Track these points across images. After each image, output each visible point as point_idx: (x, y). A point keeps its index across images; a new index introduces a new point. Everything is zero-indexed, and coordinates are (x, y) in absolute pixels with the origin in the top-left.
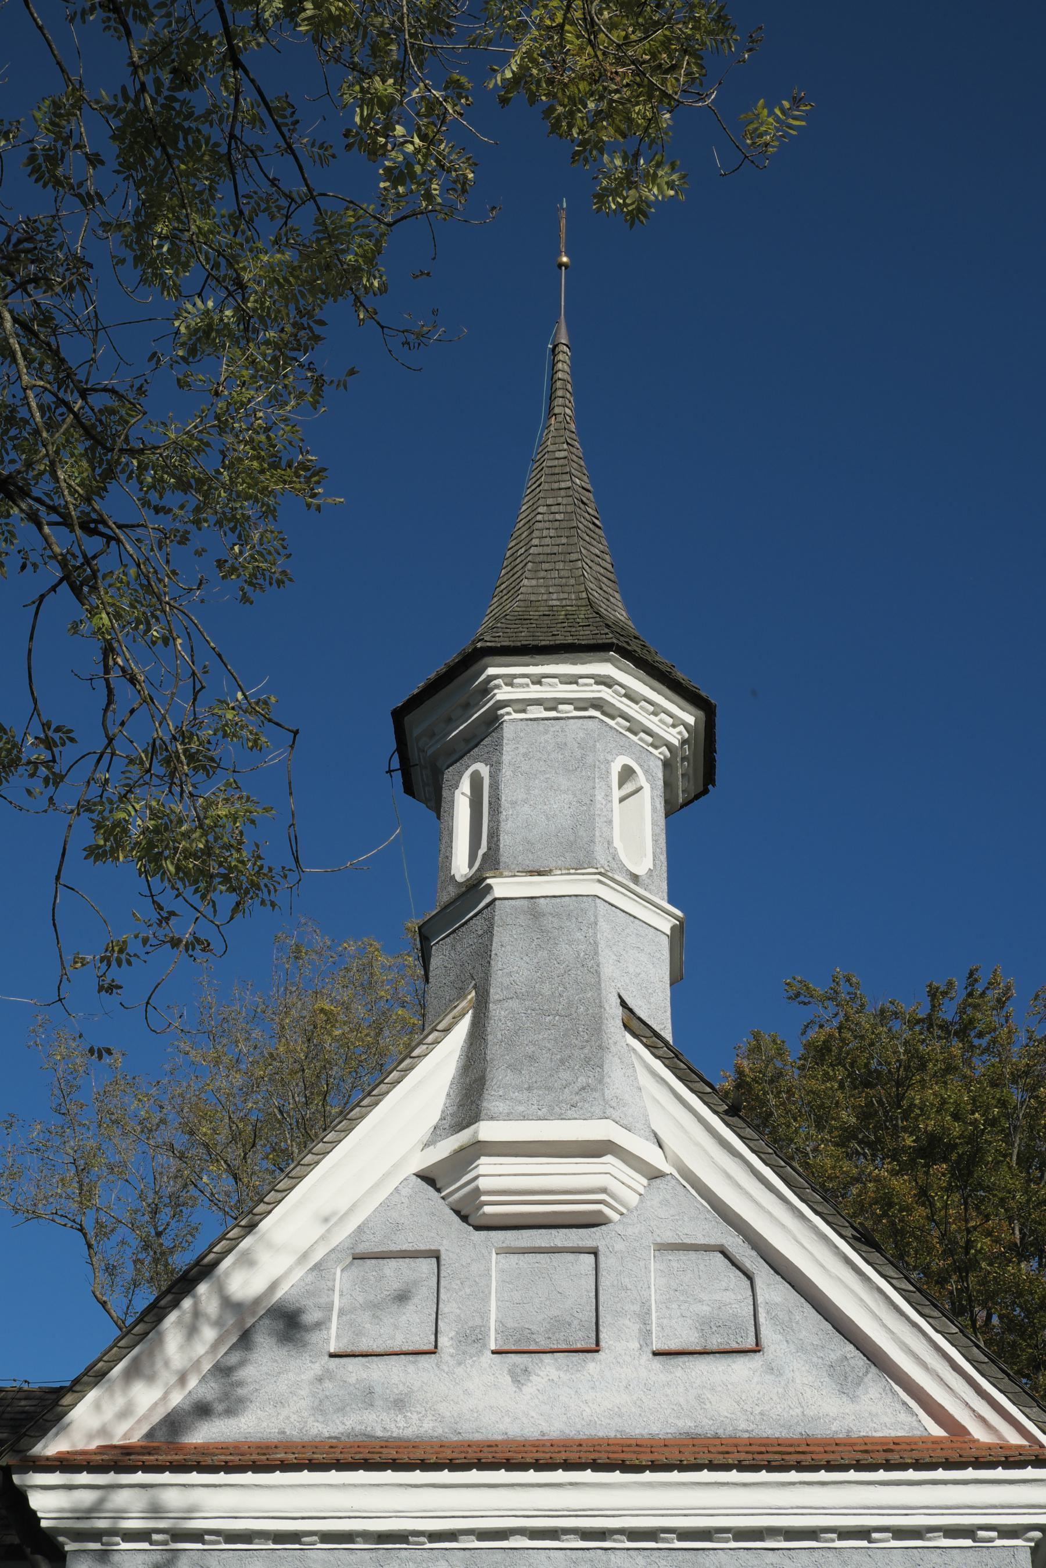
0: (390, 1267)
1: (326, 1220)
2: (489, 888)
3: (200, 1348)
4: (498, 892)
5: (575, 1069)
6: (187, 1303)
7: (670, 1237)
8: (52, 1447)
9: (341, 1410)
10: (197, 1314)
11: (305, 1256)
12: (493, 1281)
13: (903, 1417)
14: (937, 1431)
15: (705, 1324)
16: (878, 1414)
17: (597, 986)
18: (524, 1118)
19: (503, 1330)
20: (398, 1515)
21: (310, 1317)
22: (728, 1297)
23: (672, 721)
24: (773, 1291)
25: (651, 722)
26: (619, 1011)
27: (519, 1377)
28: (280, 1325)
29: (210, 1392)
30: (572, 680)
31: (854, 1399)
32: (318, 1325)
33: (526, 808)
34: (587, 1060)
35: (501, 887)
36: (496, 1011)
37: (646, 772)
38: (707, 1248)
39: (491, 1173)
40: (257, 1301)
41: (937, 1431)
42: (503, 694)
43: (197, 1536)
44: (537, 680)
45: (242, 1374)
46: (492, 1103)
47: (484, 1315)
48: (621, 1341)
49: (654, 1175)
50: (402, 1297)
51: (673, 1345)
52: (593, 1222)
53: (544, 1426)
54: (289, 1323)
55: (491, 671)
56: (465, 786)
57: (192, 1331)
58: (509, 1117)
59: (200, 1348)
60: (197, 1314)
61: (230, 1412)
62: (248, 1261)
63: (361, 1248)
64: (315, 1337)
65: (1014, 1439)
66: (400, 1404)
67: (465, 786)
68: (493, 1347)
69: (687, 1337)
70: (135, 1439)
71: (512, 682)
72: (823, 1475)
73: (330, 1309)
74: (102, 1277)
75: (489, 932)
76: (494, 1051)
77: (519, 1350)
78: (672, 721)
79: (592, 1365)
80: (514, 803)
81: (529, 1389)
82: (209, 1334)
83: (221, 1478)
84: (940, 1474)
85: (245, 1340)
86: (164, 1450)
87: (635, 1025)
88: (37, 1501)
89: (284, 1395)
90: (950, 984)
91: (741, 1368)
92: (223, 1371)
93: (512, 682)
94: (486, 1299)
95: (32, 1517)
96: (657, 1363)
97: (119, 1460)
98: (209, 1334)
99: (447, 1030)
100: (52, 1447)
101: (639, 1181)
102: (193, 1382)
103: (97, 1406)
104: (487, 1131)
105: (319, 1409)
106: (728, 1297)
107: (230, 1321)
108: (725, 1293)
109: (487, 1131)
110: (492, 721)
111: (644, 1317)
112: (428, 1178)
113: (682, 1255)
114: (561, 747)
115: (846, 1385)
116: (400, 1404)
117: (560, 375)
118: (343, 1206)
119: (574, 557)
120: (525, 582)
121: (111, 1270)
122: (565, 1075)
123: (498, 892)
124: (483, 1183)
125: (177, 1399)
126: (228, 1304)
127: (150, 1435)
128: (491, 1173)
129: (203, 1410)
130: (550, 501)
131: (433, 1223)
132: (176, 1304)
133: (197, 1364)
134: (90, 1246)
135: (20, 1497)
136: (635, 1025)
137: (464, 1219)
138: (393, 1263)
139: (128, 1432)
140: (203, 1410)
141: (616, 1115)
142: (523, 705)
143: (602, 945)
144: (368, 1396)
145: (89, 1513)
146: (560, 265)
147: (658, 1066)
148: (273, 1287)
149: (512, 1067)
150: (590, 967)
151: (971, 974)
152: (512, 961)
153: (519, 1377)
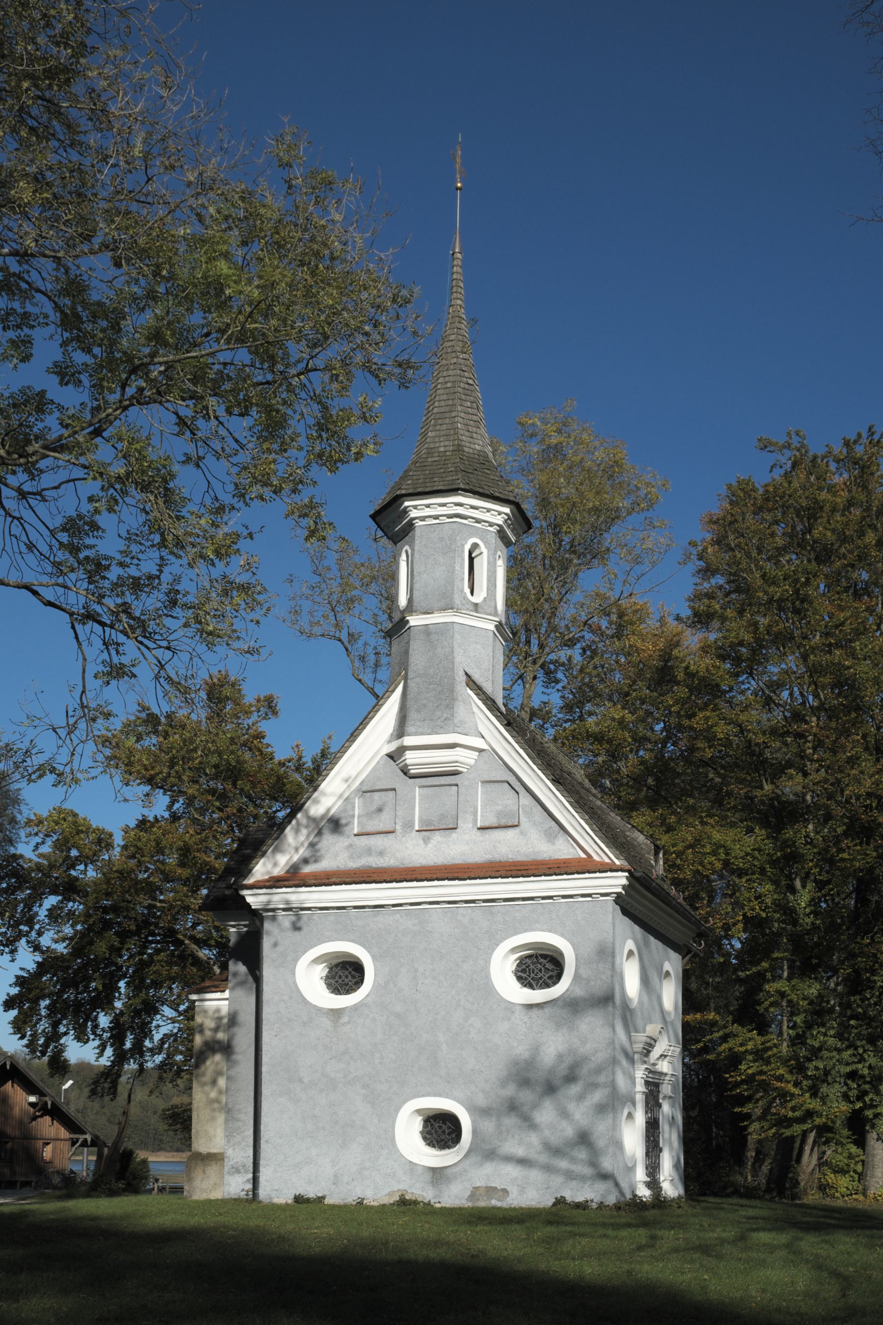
0: (376, 795)
1: (347, 781)
2: (408, 621)
3: (302, 838)
4: (412, 623)
5: (442, 713)
6: (294, 822)
7: (487, 778)
8: (250, 881)
9: (359, 857)
10: (298, 824)
11: (341, 796)
12: (418, 801)
13: (571, 850)
14: (583, 856)
15: (499, 814)
16: (562, 850)
17: (453, 669)
18: (422, 734)
19: (421, 820)
20: (378, 899)
21: (343, 822)
22: (509, 802)
23: (497, 514)
24: (525, 799)
25: (487, 517)
26: (464, 678)
27: (426, 841)
28: (331, 825)
29: (307, 854)
30: (444, 505)
31: (553, 844)
32: (346, 825)
33: (425, 576)
34: (447, 706)
35: (414, 621)
36: (411, 683)
37: (485, 543)
38: (502, 782)
39: (411, 757)
40: (323, 817)
41: (583, 856)
42: (413, 514)
43: (309, 909)
44: (428, 506)
45: (319, 846)
46: (410, 728)
47: (413, 815)
48: (466, 825)
49: (481, 751)
50: (380, 810)
51: (487, 824)
52: (455, 773)
53: (436, 860)
54: (335, 824)
55: (407, 504)
56: (404, 557)
57: (297, 831)
58: (416, 734)
59: (302, 838)
60: (298, 824)
61: (316, 861)
62: (316, 802)
63: (364, 789)
64: (347, 829)
65: (607, 860)
66: (381, 853)
67: (404, 557)
68: (417, 828)
69: (492, 821)
70: (282, 873)
71: (418, 509)
72: (532, 878)
73: (353, 816)
74: (357, 663)
75: (408, 642)
76: (410, 703)
77: (428, 830)
78: (497, 514)
79: (454, 835)
80: (419, 573)
81: (430, 846)
82: (304, 832)
83: (313, 889)
84: (576, 876)
85: (320, 833)
86: (294, 878)
87: (471, 683)
88: (249, 899)
89: (336, 854)
90: (859, 435)
91: (511, 833)
92: (312, 845)
93: (418, 509)
94: (414, 808)
95: (249, 905)
96: (479, 833)
97: (275, 883)
98: (304, 832)
99: (393, 691)
100: (250, 881)
101: (475, 755)
102: (301, 851)
103: (264, 864)
104: (408, 741)
105: (351, 857)
106: (509, 802)
107: (313, 826)
108: (507, 800)
109: (408, 741)
110: (410, 525)
111: (475, 814)
112: (391, 756)
113: (492, 785)
114: (442, 539)
115: (550, 837)
116: (381, 853)
117: (455, 276)
118: (354, 774)
119: (454, 414)
120: (430, 434)
121: (362, 659)
122: (438, 713)
123: (412, 623)
124: (408, 762)
125: (296, 858)
126: (314, 820)
127: (287, 872)
128: (411, 757)
129: (306, 861)
130: (445, 374)
131: (392, 776)
132: (290, 822)
133: (302, 844)
134: (347, 649)
135: (243, 898)
136: (471, 683)
137: (405, 774)
138: (378, 794)
139: (277, 872)
140: (306, 861)
141: (459, 730)
142: (423, 519)
143: (456, 647)
144: (369, 851)
145: (269, 902)
146: (457, 189)
147: (480, 703)
148: (329, 810)
149: (418, 711)
150: (450, 658)
151: (870, 429)
152: (418, 658)
153: (426, 841)
